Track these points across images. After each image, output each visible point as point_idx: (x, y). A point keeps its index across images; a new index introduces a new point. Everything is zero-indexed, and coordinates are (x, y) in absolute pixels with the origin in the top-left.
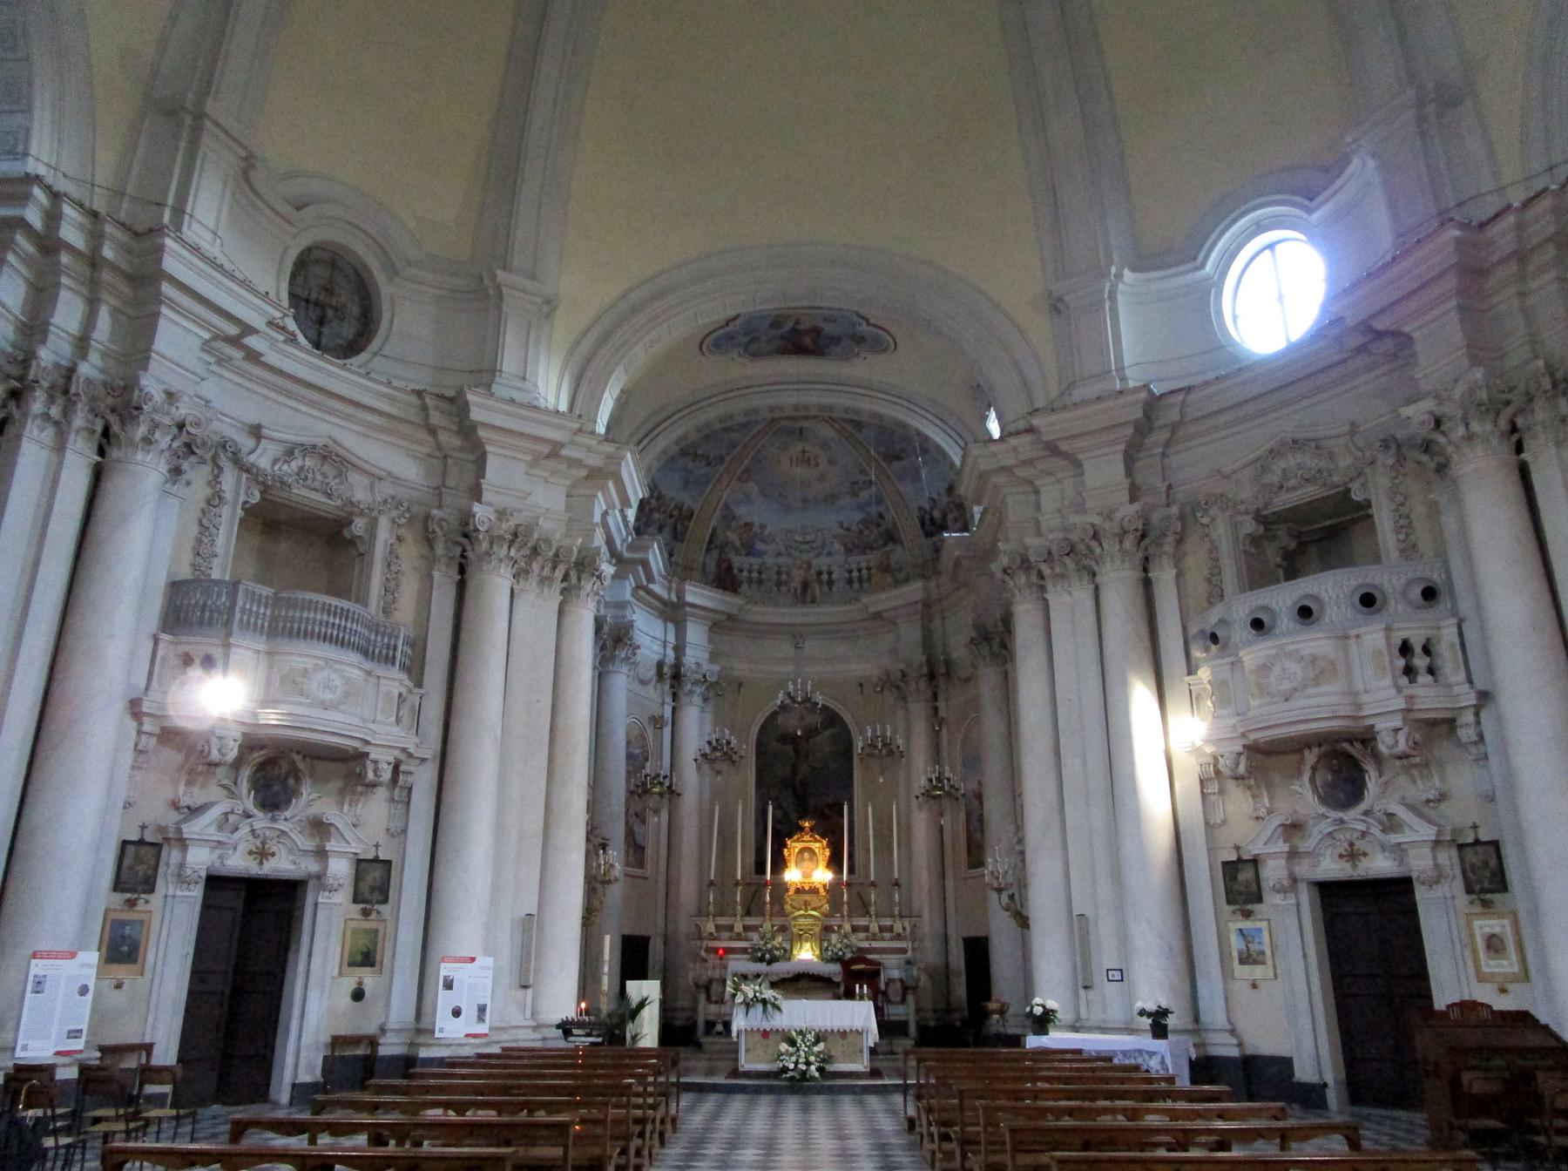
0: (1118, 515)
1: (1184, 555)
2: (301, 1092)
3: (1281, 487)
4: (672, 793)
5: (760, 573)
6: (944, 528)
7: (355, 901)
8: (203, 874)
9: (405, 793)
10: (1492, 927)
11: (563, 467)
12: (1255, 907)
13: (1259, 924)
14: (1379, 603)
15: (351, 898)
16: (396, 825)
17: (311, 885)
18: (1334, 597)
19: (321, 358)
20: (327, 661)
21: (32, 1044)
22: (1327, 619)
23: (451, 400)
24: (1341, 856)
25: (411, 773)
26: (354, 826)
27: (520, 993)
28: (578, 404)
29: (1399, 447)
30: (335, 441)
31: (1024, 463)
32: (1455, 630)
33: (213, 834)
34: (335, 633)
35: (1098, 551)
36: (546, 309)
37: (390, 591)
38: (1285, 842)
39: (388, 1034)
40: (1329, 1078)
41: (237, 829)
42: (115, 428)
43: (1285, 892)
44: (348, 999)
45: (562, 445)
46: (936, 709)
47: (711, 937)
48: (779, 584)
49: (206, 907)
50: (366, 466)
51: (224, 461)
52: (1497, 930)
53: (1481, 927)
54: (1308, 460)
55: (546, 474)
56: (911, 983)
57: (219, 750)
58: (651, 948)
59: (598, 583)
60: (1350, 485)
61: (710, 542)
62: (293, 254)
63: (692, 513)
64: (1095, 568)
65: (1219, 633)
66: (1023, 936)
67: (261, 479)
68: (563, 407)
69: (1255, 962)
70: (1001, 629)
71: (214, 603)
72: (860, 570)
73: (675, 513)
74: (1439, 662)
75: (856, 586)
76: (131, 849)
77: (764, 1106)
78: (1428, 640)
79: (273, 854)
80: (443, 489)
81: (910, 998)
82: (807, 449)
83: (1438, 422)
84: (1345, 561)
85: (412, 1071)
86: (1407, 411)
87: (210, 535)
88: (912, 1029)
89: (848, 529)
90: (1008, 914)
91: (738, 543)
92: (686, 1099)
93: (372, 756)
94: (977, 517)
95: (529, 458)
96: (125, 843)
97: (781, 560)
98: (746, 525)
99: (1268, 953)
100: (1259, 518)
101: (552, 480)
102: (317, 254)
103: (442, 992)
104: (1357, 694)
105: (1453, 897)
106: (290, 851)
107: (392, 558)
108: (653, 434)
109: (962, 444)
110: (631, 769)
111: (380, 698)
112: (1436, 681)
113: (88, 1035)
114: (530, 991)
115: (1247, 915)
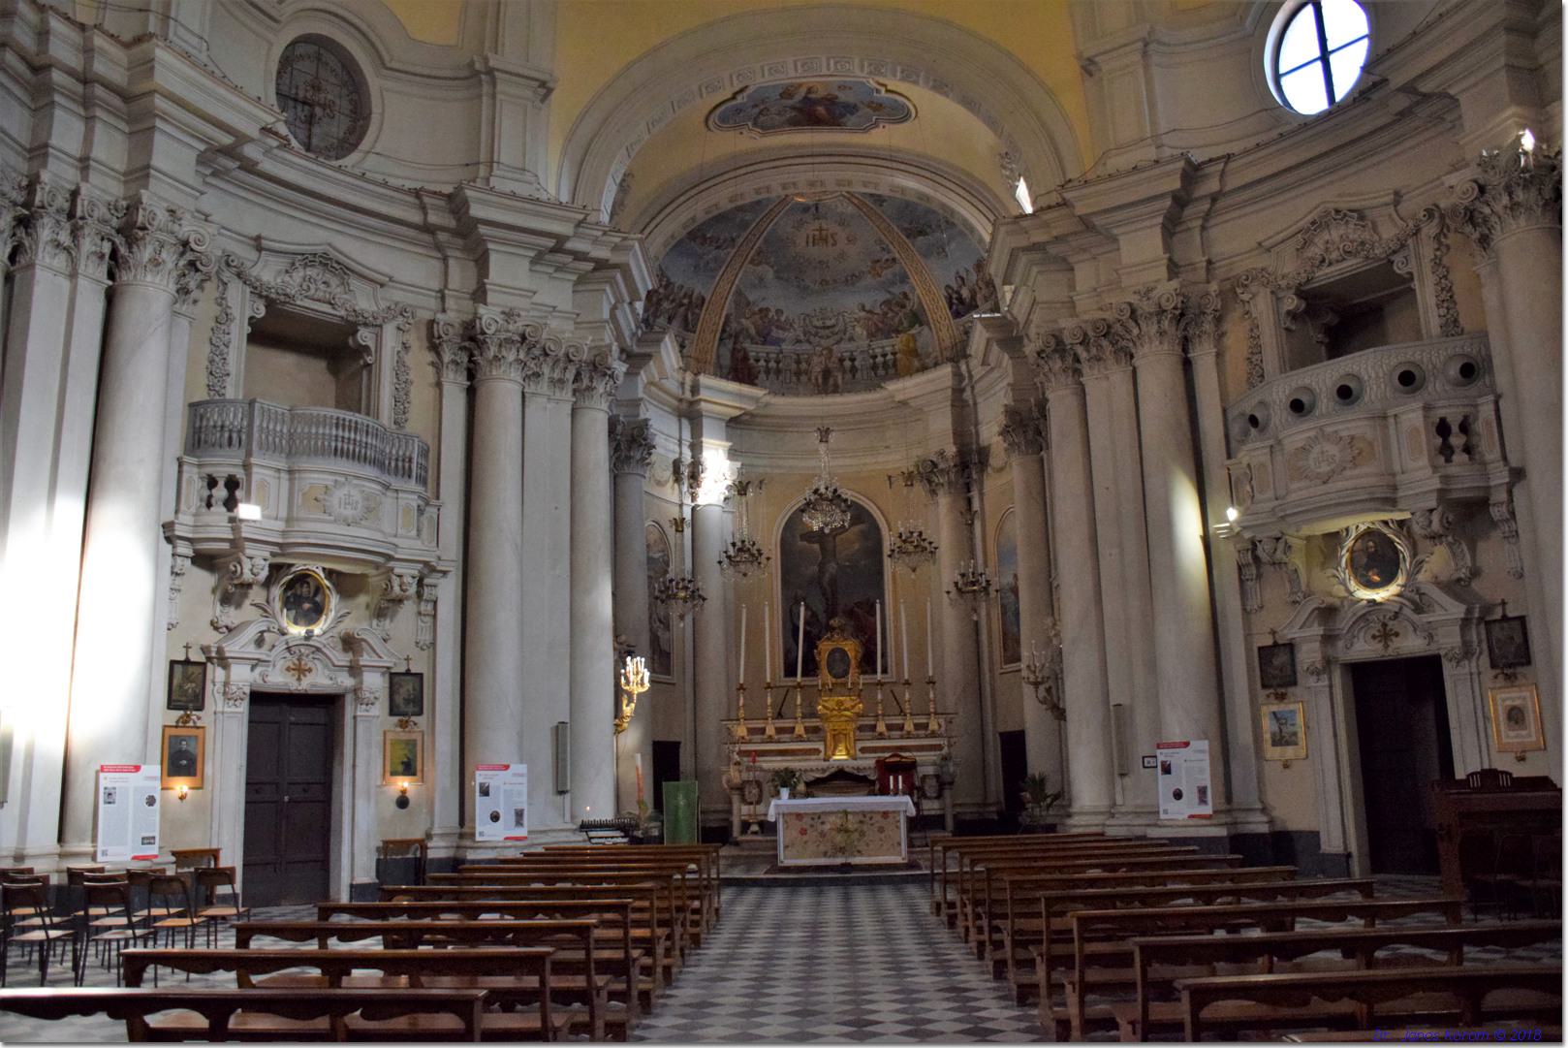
0: (1155, 294)
1: (1223, 334)
2: (356, 890)
3: (1323, 261)
4: (696, 596)
5: (778, 362)
6: (974, 307)
7: (392, 713)
8: (248, 691)
9: (430, 607)
10: (1513, 699)
11: (568, 259)
12: (1290, 690)
13: (1292, 707)
14: (1417, 382)
15: (387, 710)
16: (426, 638)
17: (349, 699)
18: (1373, 376)
19: (315, 161)
20: (346, 476)
21: (111, 850)
22: (1366, 399)
23: (449, 197)
24: (1374, 637)
25: (435, 586)
26: (385, 640)
27: (559, 798)
28: (580, 195)
29: (1442, 217)
30: (335, 249)
31: (1058, 239)
32: (1492, 407)
33: (252, 652)
34: (351, 448)
35: (1136, 331)
36: (542, 91)
37: (401, 402)
38: (1320, 625)
39: (435, 839)
40: (1353, 848)
41: (274, 646)
42: (123, 250)
43: (1318, 674)
44: (393, 807)
45: (567, 238)
46: (969, 501)
47: (743, 740)
48: (798, 374)
49: (252, 722)
50: (366, 272)
51: (226, 275)
52: (1517, 703)
53: (1504, 700)
54: (1353, 232)
55: (551, 270)
56: (947, 779)
57: (251, 570)
58: (681, 751)
59: (611, 382)
60: (1392, 258)
61: (724, 331)
62: (277, 52)
63: (703, 300)
64: (1133, 351)
65: (1258, 415)
66: (1060, 725)
67: (265, 293)
68: (565, 198)
69: (1288, 744)
70: (1036, 414)
71: (232, 423)
72: (884, 355)
73: (686, 301)
74: (1475, 440)
75: (881, 372)
76: (178, 669)
77: (805, 898)
78: (1466, 418)
79: (310, 670)
80: (446, 292)
81: (947, 793)
82: (824, 226)
83: (1482, 189)
84: (1380, 340)
85: (461, 867)
86: (1452, 180)
87: (222, 354)
88: (950, 822)
89: (870, 312)
90: (1044, 706)
91: (753, 331)
92: (727, 895)
93: (397, 571)
94: (1008, 296)
95: (532, 254)
96: (173, 663)
97: (798, 348)
98: (761, 310)
99: (1301, 735)
100: (1301, 293)
101: (555, 275)
102: (300, 50)
103: (478, 798)
104: (1394, 475)
105: (1479, 673)
106: (326, 666)
107: (401, 366)
108: (658, 220)
109: (992, 218)
110: (652, 574)
111: (400, 512)
112: (1471, 459)
113: (160, 839)
114: (568, 796)
115: (1281, 697)
